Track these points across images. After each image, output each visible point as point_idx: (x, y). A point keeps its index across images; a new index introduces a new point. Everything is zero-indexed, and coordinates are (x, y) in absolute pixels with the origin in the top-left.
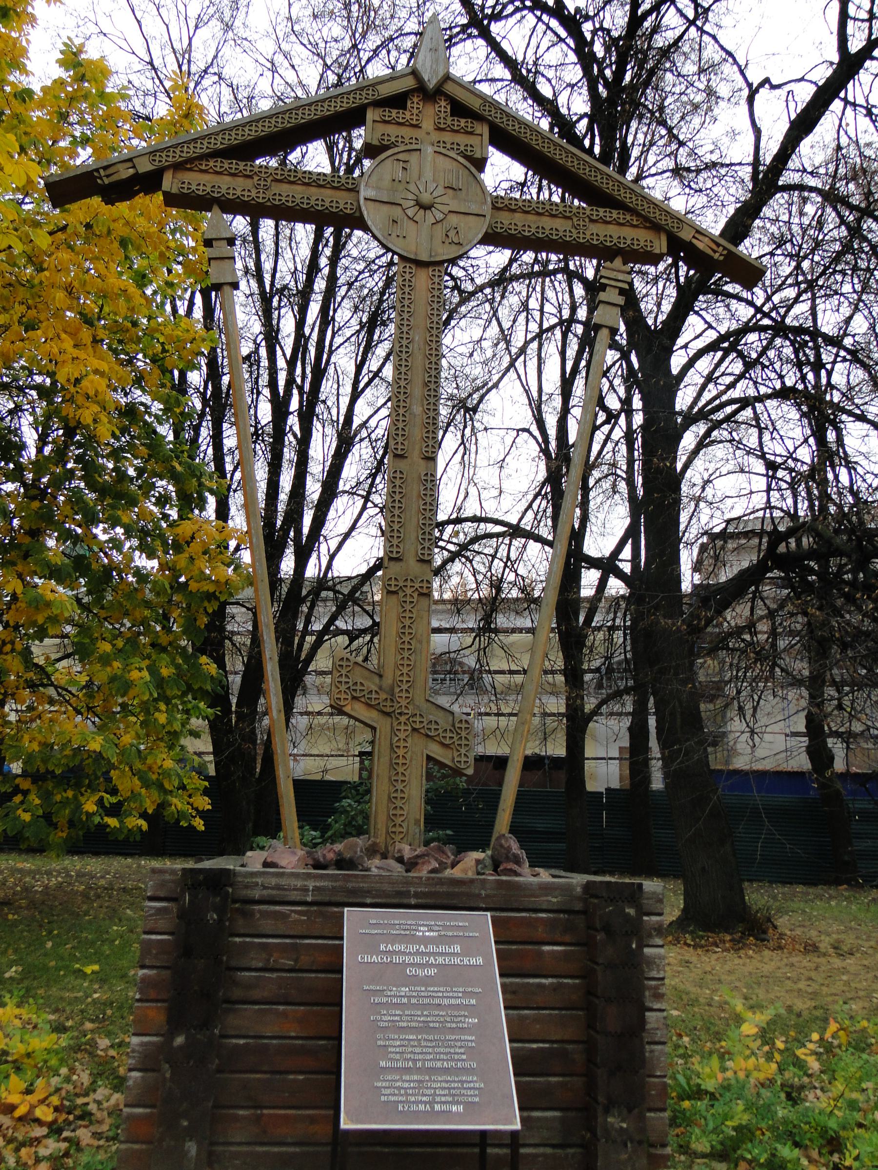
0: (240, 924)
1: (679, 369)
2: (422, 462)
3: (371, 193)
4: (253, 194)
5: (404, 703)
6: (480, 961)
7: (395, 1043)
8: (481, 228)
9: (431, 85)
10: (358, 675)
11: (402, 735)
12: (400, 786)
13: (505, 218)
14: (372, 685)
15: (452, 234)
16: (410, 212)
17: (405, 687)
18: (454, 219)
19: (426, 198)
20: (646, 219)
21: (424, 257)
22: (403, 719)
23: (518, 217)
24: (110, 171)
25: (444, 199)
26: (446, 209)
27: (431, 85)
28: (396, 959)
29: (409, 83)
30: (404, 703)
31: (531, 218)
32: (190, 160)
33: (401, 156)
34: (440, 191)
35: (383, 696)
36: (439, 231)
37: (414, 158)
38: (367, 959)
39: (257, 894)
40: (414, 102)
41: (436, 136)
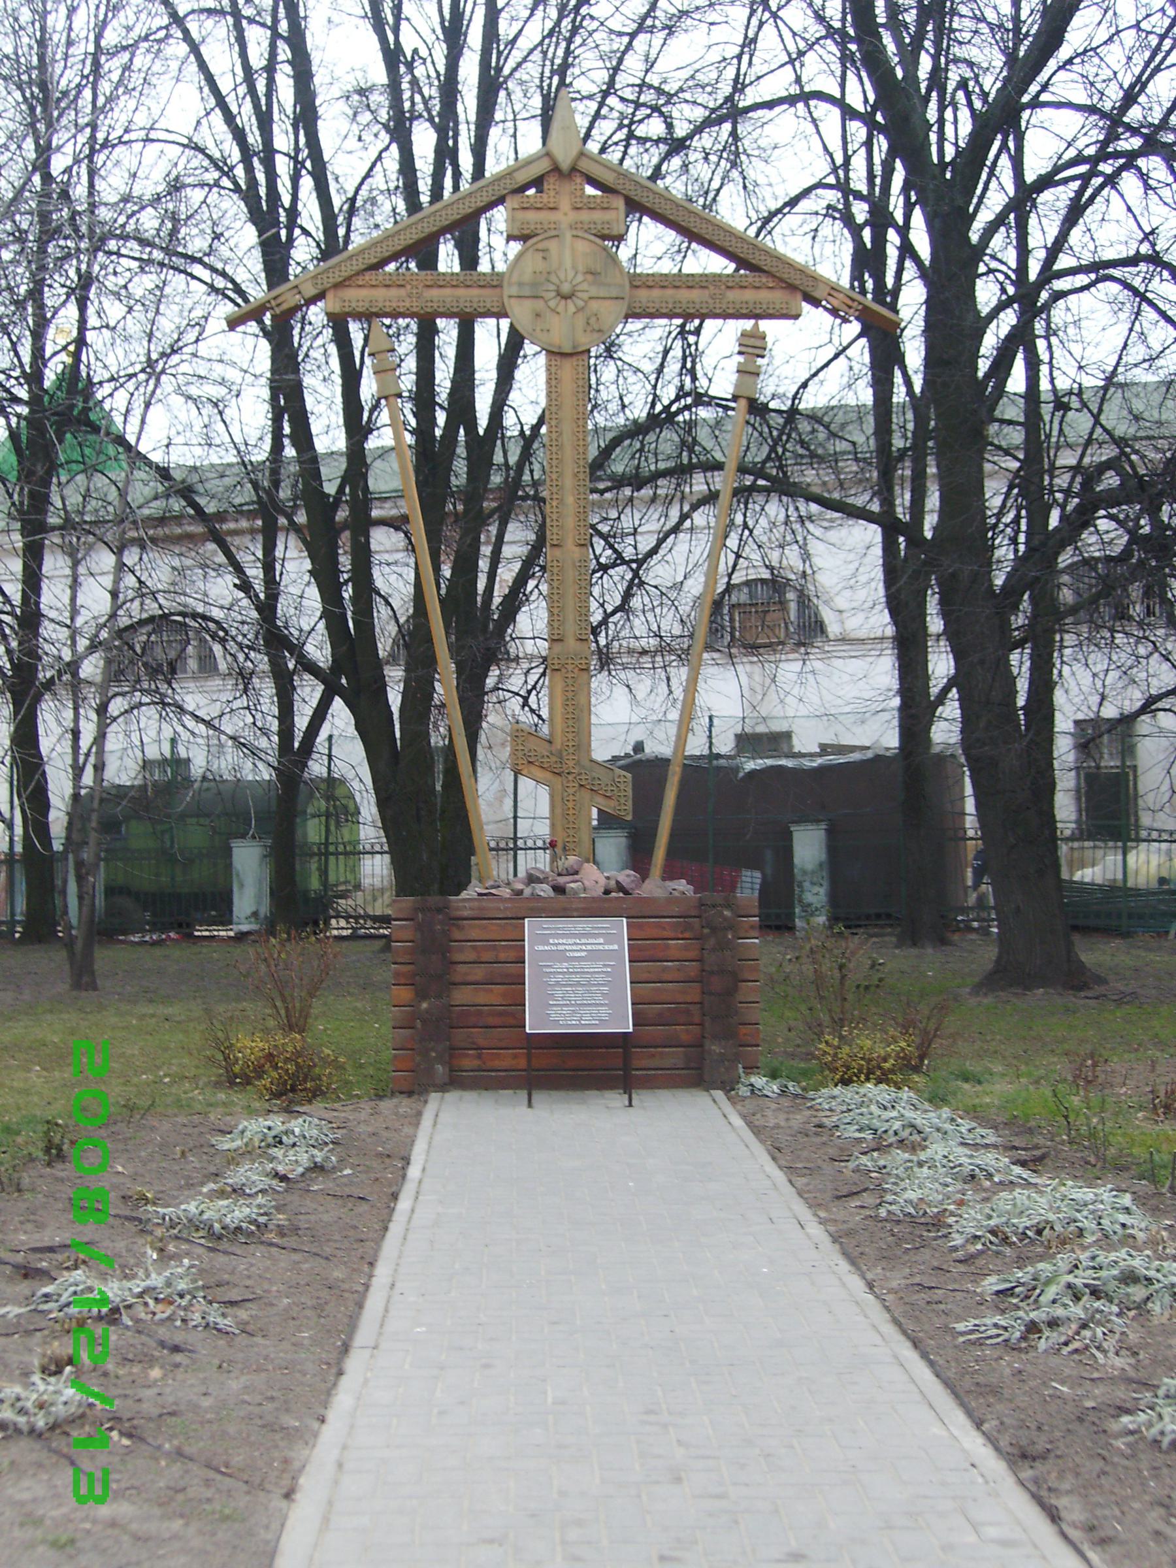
0: (457, 935)
1: (1034, 177)
2: (577, 549)
3: (514, 291)
4: (408, 305)
5: (571, 764)
6: (616, 947)
7: (559, 993)
8: (622, 308)
9: (565, 165)
10: (532, 744)
11: (571, 791)
12: (571, 832)
13: (643, 294)
14: (543, 749)
15: (593, 320)
16: (552, 304)
17: (571, 750)
18: (594, 305)
19: (566, 288)
20: (781, 280)
21: (567, 349)
22: (570, 777)
23: (656, 293)
24: (279, 301)
25: (585, 286)
26: (585, 296)
27: (565, 165)
28: (561, 948)
29: (544, 166)
30: (571, 764)
31: (670, 292)
32: (349, 278)
33: (540, 246)
34: (580, 278)
35: (554, 759)
36: (580, 321)
37: (552, 245)
38: (541, 948)
39: (466, 913)
40: (550, 184)
41: (573, 216)
